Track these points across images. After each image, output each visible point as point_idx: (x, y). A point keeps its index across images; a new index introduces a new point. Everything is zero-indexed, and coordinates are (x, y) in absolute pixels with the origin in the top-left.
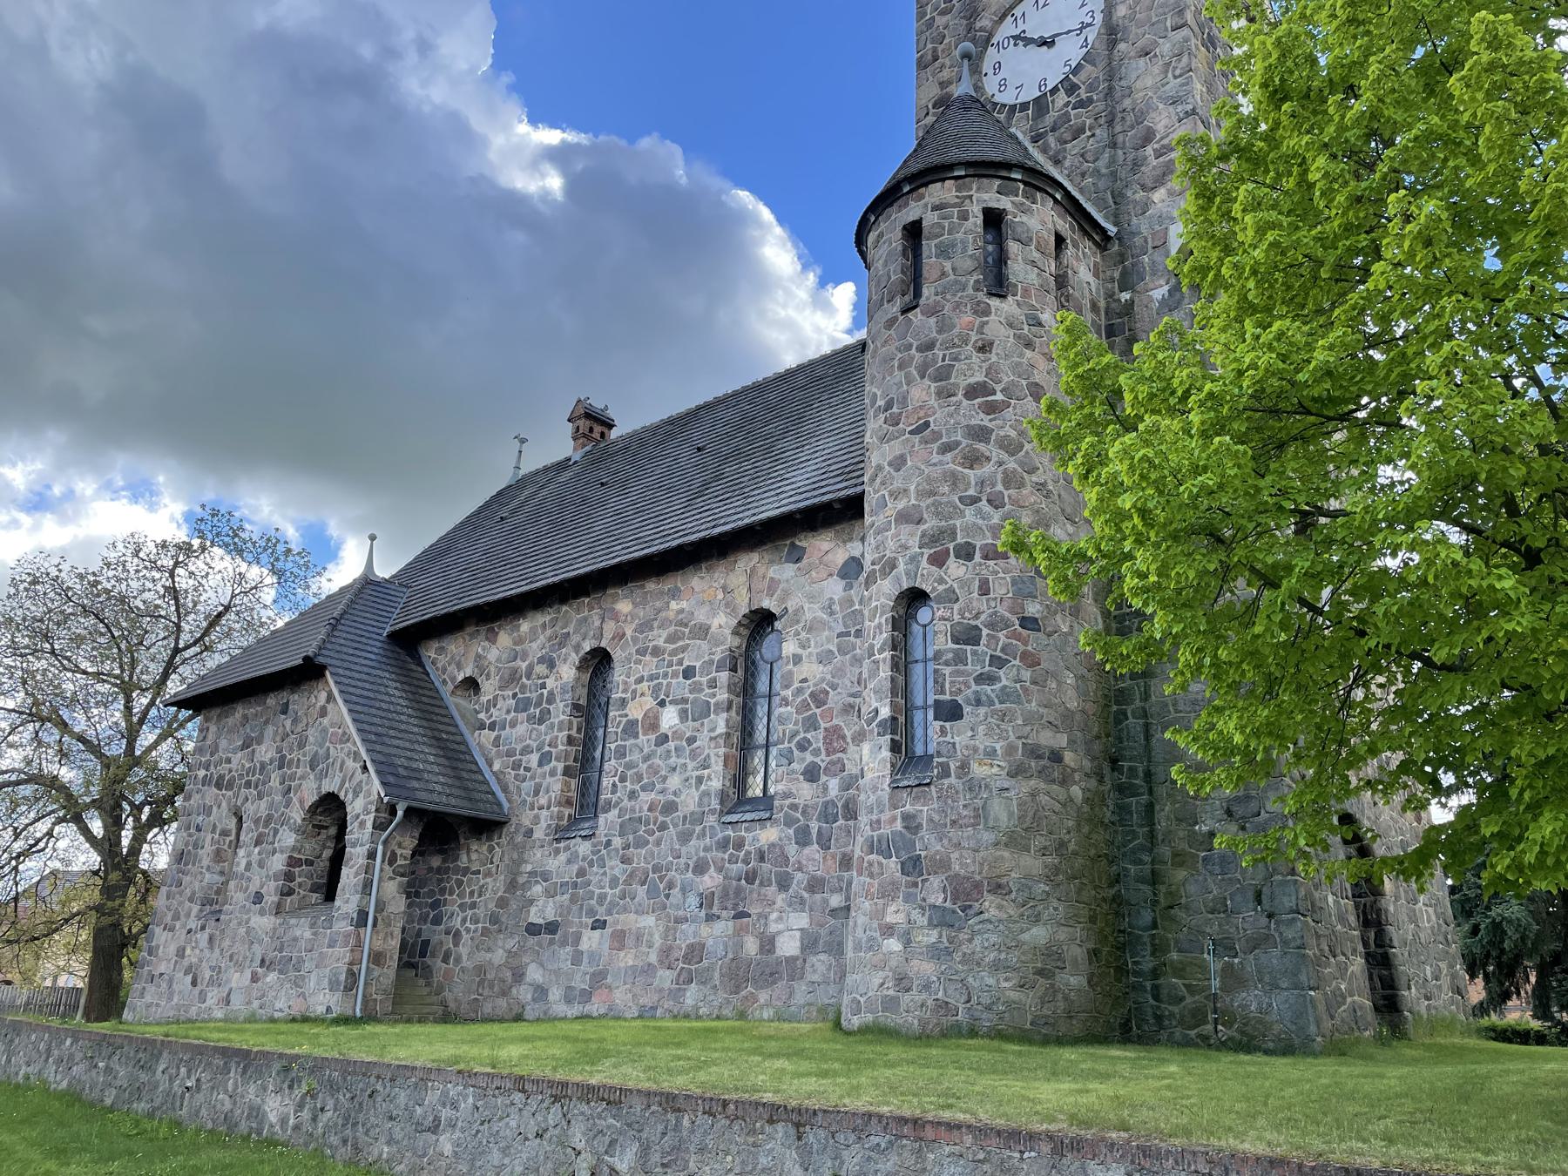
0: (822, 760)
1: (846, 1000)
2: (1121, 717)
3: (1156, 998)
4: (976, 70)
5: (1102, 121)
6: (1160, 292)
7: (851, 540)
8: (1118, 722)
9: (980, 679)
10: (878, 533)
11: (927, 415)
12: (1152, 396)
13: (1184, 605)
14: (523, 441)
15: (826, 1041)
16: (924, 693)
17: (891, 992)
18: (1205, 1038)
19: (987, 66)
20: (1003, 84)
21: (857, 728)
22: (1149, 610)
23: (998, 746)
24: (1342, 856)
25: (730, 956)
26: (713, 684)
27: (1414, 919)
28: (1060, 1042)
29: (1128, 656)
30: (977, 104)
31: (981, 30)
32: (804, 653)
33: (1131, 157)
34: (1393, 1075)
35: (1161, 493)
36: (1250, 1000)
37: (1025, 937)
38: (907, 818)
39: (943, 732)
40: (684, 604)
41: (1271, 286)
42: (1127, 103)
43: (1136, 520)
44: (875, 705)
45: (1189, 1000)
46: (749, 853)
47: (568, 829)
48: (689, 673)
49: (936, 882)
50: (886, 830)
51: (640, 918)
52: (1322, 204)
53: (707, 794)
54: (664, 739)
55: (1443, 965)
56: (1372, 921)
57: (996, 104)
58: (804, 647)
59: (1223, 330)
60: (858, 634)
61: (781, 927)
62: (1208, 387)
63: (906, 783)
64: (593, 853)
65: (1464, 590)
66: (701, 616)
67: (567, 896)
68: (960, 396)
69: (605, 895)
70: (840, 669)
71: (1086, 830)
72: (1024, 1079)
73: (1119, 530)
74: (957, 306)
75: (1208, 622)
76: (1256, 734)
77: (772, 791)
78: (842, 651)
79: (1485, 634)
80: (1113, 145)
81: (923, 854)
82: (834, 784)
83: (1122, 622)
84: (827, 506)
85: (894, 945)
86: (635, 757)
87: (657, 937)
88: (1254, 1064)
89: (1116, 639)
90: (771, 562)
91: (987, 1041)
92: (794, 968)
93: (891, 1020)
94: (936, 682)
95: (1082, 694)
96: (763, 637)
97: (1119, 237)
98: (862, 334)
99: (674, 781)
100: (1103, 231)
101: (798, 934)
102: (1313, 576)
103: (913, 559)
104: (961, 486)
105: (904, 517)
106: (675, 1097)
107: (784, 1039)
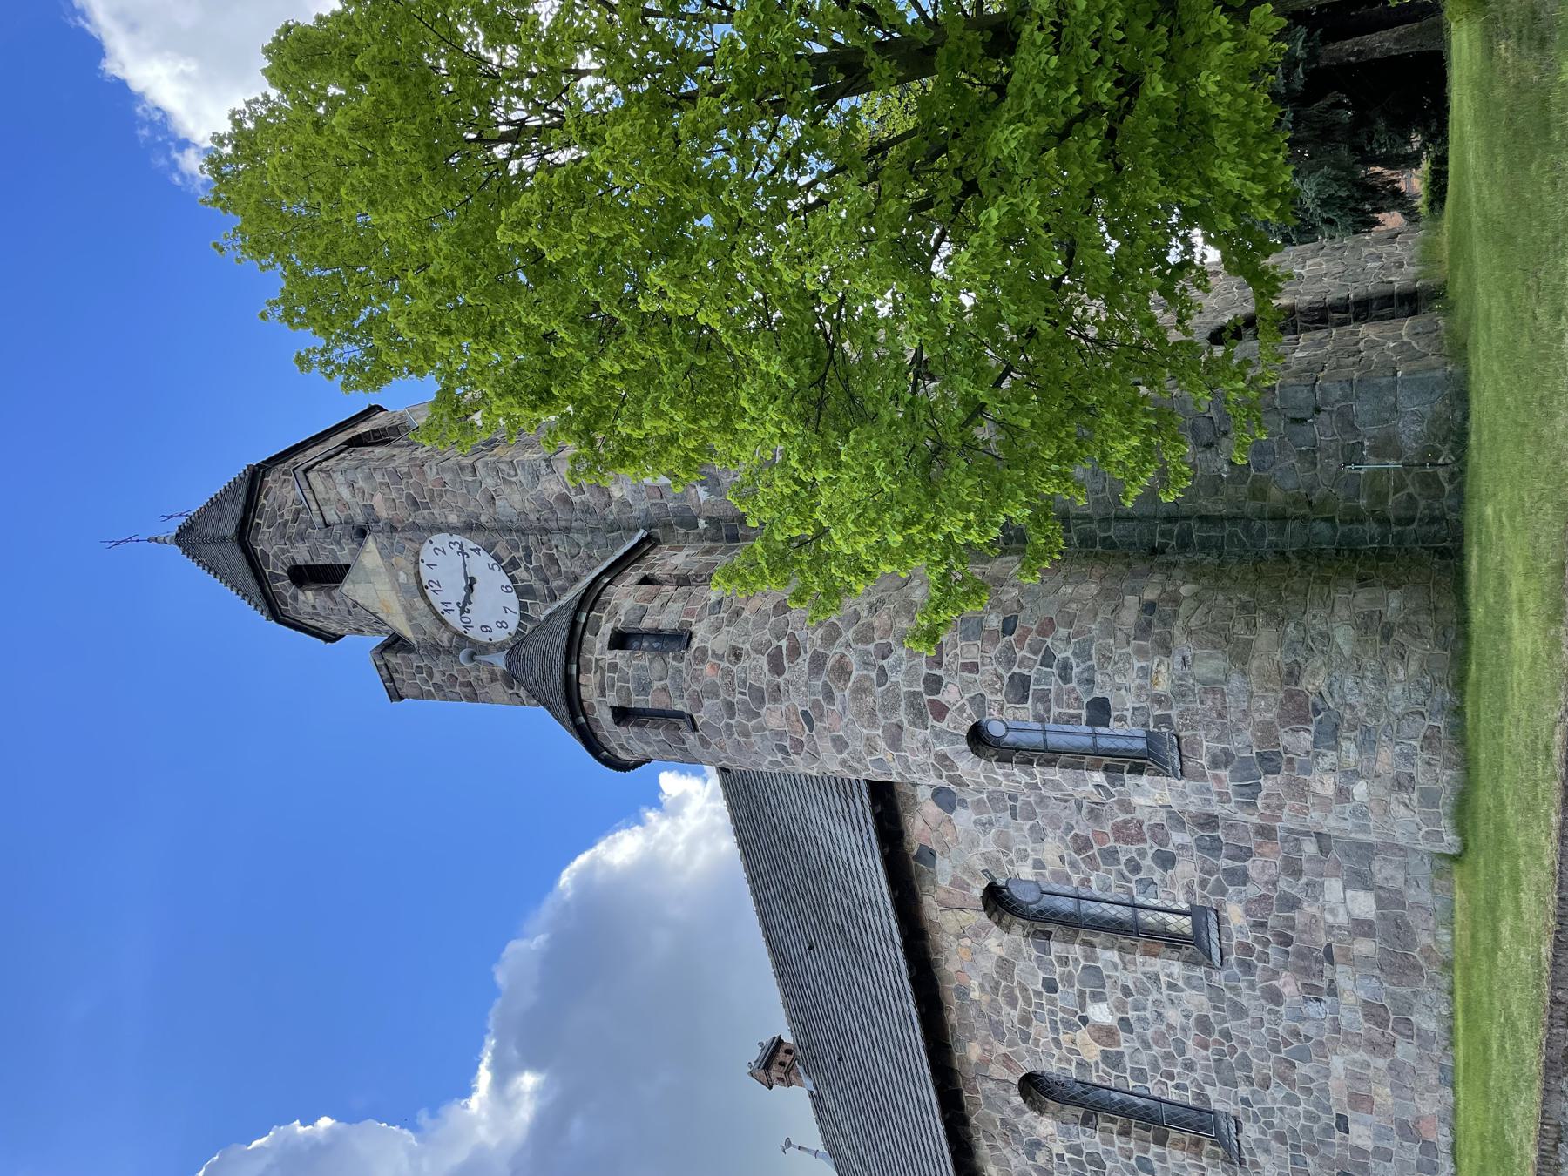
0: (1150, 848)
1: (1424, 846)
2: (1108, 543)
3: (1411, 521)
4: (484, 648)
5: (545, 538)
6: (703, 494)
7: (914, 797)
8: (1113, 545)
9: (1065, 675)
10: (909, 770)
11: (796, 713)
12: (797, 512)
13: (999, 489)
14: (789, 1144)
15: (1475, 874)
16: (1079, 735)
17: (1415, 796)
18: (1452, 477)
19: (483, 638)
20: (502, 624)
21: (1115, 807)
22: (1002, 519)
23: (1138, 665)
24: (1255, 343)
25: (1377, 972)
26: (1064, 961)
27: (1319, 278)
28: (1464, 621)
29: (1047, 537)
30: (515, 649)
31: (450, 642)
32: (1032, 856)
33: (579, 515)
34: (1486, 298)
35: (889, 508)
36: (1409, 432)
37: (1347, 650)
38: (1215, 763)
39: (1121, 719)
40: (975, 983)
41: (708, 406)
42: (532, 517)
43: (913, 531)
44: (1090, 787)
45: (1411, 490)
46: (1256, 939)
47: (1228, 1148)
48: (1051, 986)
49: (1287, 739)
50: (1230, 787)
51: (1335, 1073)
52: (643, 363)
53: (1188, 980)
54: (1124, 1022)
55: (1366, 251)
56: (1320, 316)
57: (518, 632)
58: (1026, 856)
59: (743, 447)
60: (1013, 797)
61: (1341, 910)
62: (794, 464)
63: (1177, 762)
64: (1257, 1121)
65: (999, 249)
66: (988, 966)
67: (1309, 1159)
68: (781, 680)
69: (1306, 1112)
70: (1051, 819)
71: (1227, 582)
72: (1510, 663)
73: (922, 546)
74: (695, 678)
75: (1017, 467)
76: (1130, 424)
77: (1185, 906)
78: (1031, 815)
79: (1040, 232)
80: (567, 530)
81: (1255, 750)
82: (1177, 838)
83: (1013, 540)
84: (879, 819)
85: (1360, 789)
86: (1144, 1059)
87: (1356, 1056)
88: (1479, 432)
89: (1029, 548)
90: (933, 883)
91: (1467, 698)
92: (1389, 901)
93: (1447, 798)
94: (1067, 722)
95: (1082, 579)
96: (1013, 900)
97: (648, 527)
98: (711, 771)
99: (1173, 1016)
100: (642, 541)
101: (1349, 893)
102: (977, 376)
103: (937, 736)
104: (867, 684)
105: (895, 742)
106: (1550, 1060)
107: (1474, 921)
